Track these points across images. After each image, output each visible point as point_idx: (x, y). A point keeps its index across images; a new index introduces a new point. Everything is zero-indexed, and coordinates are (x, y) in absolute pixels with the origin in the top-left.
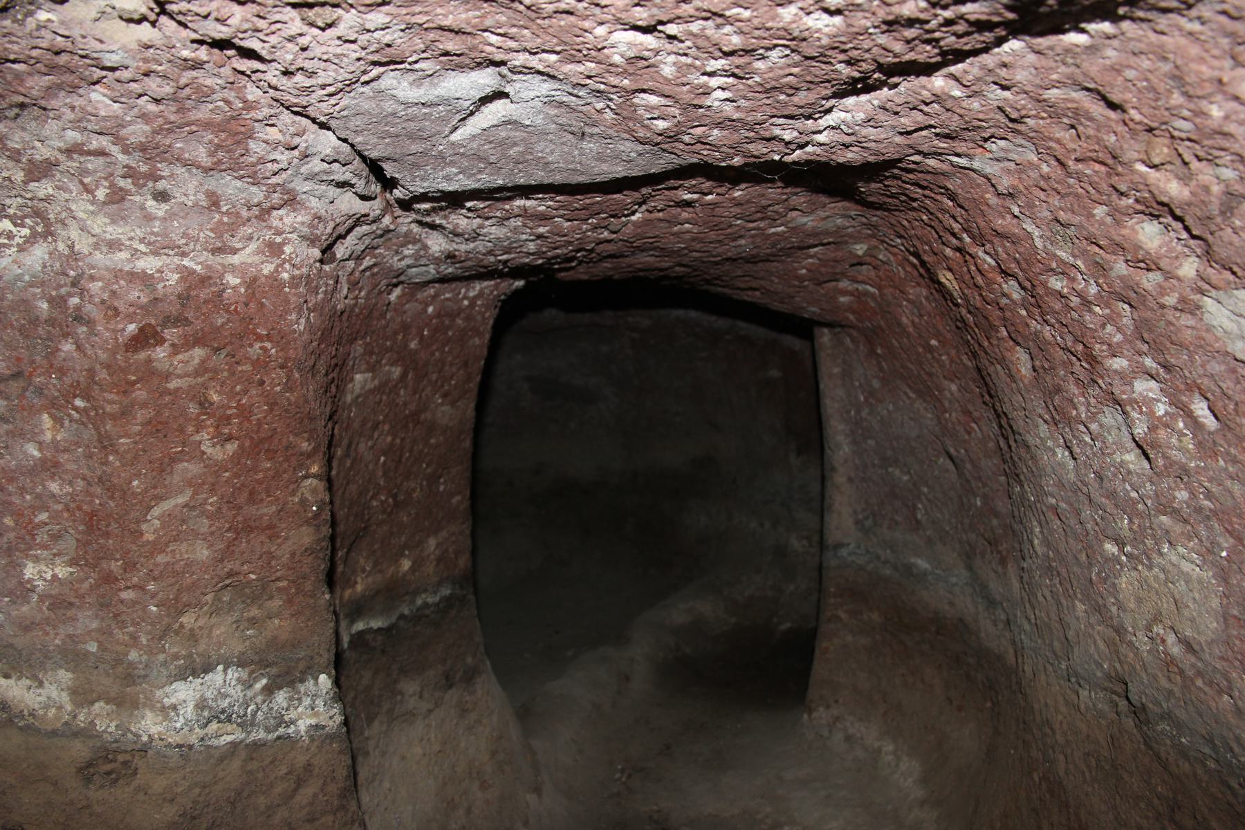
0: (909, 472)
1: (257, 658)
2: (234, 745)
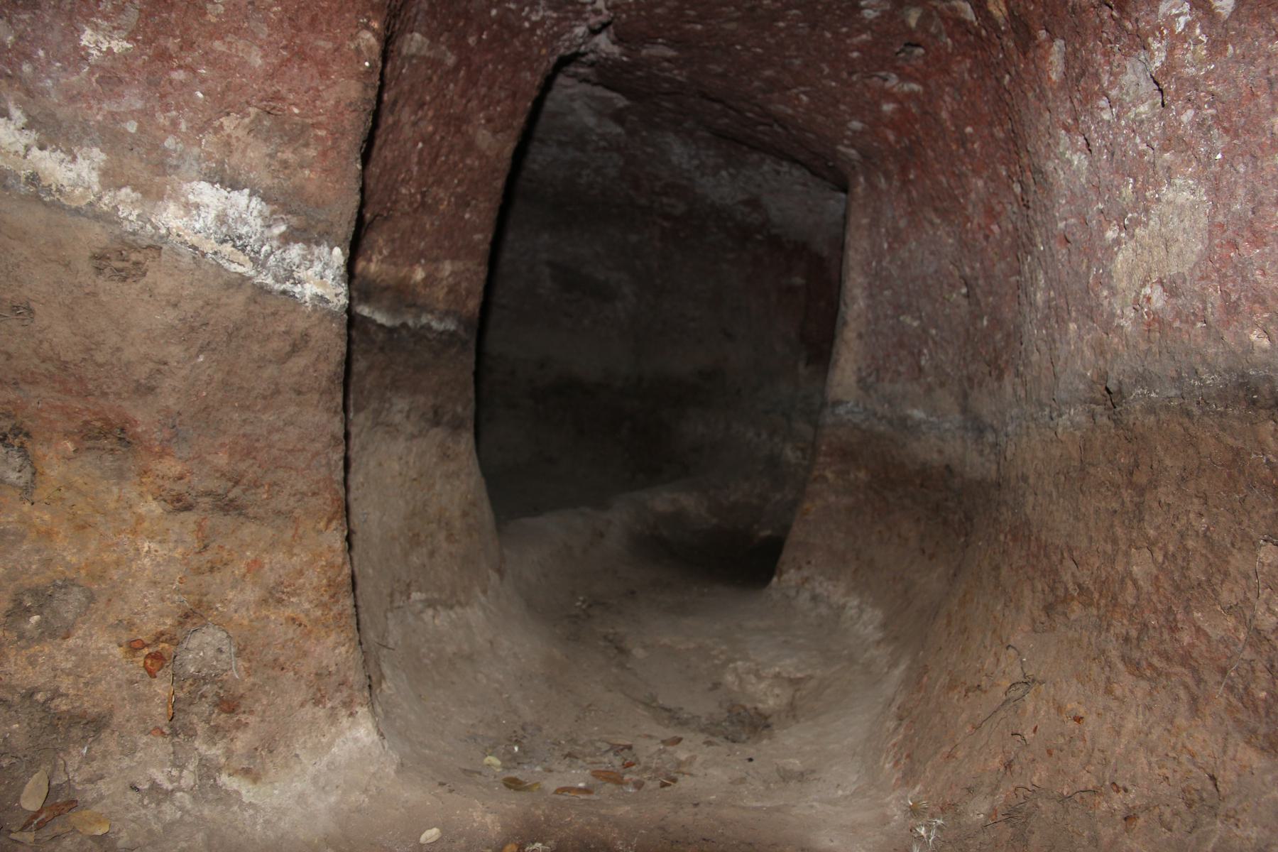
0: (920, 318)
1: (281, 200)
2: (243, 279)
